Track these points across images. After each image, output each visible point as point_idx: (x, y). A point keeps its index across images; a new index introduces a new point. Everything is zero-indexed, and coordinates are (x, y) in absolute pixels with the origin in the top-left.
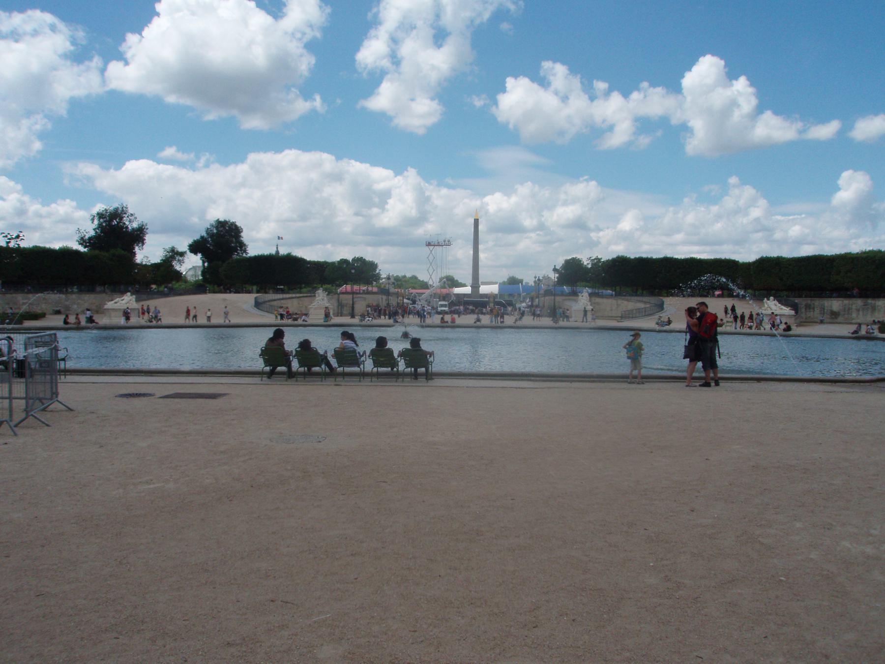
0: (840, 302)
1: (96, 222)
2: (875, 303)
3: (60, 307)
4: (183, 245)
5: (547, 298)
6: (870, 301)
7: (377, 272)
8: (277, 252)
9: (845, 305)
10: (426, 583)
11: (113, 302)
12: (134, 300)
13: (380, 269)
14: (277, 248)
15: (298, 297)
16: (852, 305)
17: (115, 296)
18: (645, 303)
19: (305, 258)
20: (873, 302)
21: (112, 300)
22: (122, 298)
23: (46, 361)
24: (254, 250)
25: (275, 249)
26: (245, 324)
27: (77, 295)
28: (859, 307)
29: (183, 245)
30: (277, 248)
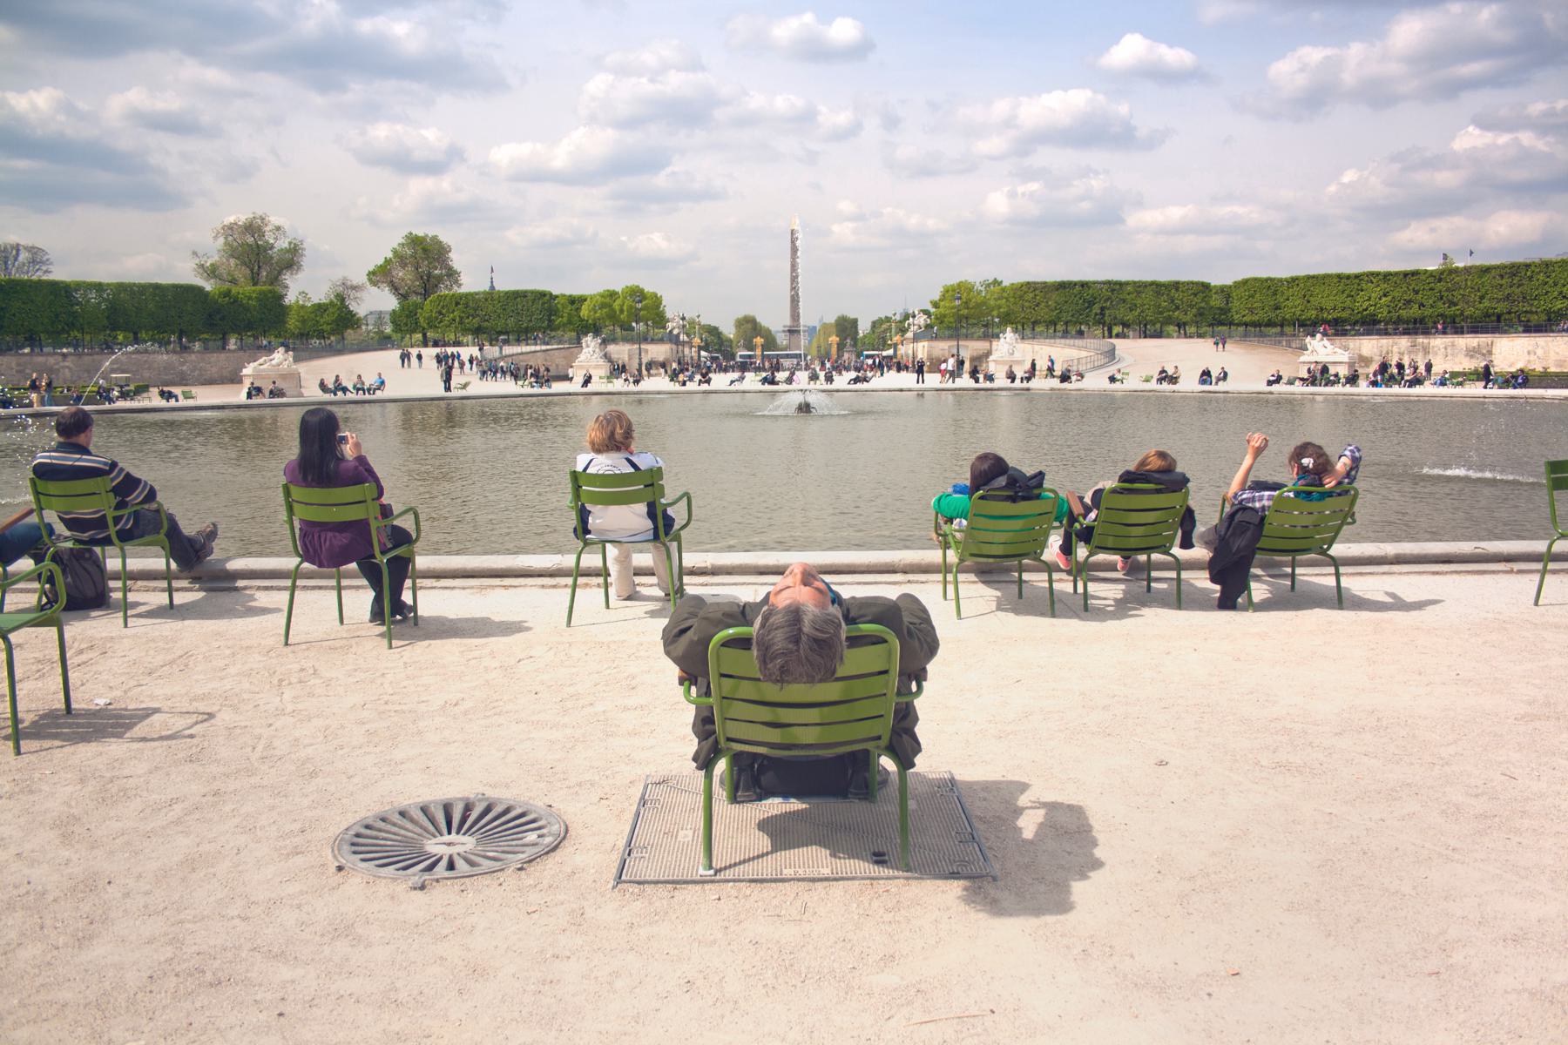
0: (1374, 341)
1: (221, 240)
2: (1429, 343)
3: (172, 374)
4: (360, 277)
5: (920, 345)
6: (1421, 340)
7: (661, 309)
8: (492, 287)
9: (1381, 347)
10: (710, 994)
11: (256, 364)
12: (291, 359)
13: (1493, 359)
14: (492, 282)
15: (544, 351)
16: (1392, 346)
17: (259, 355)
18: (1080, 348)
19: (159, 282)
20: (1426, 341)
21: (255, 361)
22: (271, 357)
23: (347, 327)
24: (471, 282)
25: (490, 284)
26: (488, 570)
27: (199, 355)
28: (1402, 350)
29: (360, 277)
30: (492, 282)
